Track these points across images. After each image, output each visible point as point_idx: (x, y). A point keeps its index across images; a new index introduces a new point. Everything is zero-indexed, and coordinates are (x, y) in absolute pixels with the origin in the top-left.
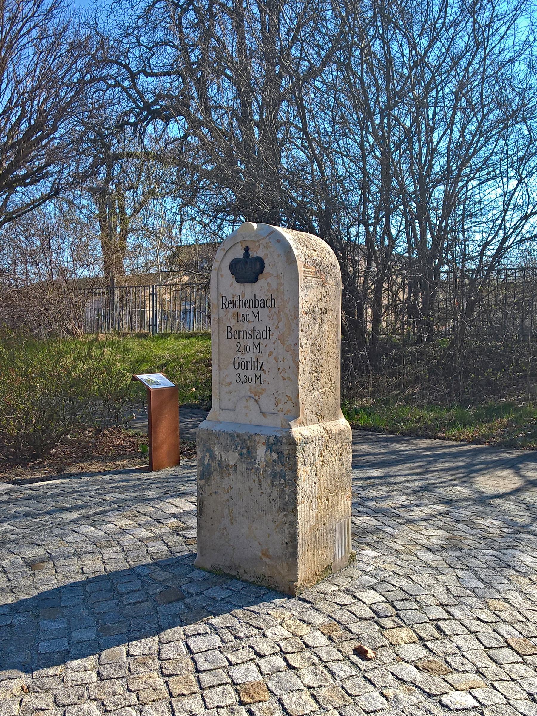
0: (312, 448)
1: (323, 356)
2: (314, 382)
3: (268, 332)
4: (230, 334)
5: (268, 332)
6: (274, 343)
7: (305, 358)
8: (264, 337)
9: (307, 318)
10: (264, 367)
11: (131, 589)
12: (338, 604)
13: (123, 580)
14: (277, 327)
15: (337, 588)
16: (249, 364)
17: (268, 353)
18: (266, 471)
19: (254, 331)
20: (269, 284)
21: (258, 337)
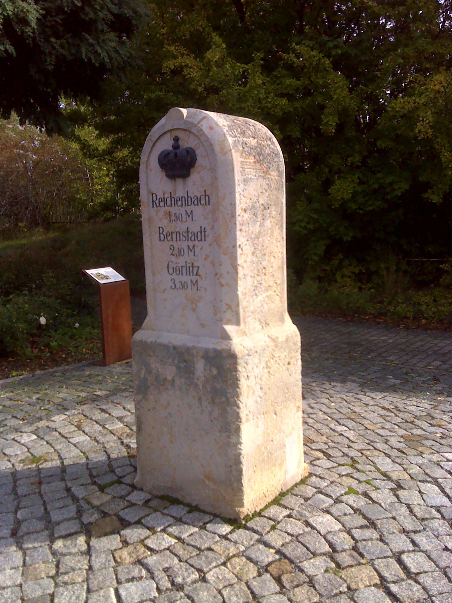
0: (256, 361)
1: (266, 257)
2: (256, 286)
3: (203, 233)
4: (162, 236)
5: (203, 233)
6: (210, 245)
8: (199, 239)
9: (246, 216)
10: (200, 272)
12: (289, 534)
13: (58, 505)
14: (213, 227)
15: (287, 512)
16: (184, 269)
17: (204, 257)
19: (188, 232)
21: (193, 239)
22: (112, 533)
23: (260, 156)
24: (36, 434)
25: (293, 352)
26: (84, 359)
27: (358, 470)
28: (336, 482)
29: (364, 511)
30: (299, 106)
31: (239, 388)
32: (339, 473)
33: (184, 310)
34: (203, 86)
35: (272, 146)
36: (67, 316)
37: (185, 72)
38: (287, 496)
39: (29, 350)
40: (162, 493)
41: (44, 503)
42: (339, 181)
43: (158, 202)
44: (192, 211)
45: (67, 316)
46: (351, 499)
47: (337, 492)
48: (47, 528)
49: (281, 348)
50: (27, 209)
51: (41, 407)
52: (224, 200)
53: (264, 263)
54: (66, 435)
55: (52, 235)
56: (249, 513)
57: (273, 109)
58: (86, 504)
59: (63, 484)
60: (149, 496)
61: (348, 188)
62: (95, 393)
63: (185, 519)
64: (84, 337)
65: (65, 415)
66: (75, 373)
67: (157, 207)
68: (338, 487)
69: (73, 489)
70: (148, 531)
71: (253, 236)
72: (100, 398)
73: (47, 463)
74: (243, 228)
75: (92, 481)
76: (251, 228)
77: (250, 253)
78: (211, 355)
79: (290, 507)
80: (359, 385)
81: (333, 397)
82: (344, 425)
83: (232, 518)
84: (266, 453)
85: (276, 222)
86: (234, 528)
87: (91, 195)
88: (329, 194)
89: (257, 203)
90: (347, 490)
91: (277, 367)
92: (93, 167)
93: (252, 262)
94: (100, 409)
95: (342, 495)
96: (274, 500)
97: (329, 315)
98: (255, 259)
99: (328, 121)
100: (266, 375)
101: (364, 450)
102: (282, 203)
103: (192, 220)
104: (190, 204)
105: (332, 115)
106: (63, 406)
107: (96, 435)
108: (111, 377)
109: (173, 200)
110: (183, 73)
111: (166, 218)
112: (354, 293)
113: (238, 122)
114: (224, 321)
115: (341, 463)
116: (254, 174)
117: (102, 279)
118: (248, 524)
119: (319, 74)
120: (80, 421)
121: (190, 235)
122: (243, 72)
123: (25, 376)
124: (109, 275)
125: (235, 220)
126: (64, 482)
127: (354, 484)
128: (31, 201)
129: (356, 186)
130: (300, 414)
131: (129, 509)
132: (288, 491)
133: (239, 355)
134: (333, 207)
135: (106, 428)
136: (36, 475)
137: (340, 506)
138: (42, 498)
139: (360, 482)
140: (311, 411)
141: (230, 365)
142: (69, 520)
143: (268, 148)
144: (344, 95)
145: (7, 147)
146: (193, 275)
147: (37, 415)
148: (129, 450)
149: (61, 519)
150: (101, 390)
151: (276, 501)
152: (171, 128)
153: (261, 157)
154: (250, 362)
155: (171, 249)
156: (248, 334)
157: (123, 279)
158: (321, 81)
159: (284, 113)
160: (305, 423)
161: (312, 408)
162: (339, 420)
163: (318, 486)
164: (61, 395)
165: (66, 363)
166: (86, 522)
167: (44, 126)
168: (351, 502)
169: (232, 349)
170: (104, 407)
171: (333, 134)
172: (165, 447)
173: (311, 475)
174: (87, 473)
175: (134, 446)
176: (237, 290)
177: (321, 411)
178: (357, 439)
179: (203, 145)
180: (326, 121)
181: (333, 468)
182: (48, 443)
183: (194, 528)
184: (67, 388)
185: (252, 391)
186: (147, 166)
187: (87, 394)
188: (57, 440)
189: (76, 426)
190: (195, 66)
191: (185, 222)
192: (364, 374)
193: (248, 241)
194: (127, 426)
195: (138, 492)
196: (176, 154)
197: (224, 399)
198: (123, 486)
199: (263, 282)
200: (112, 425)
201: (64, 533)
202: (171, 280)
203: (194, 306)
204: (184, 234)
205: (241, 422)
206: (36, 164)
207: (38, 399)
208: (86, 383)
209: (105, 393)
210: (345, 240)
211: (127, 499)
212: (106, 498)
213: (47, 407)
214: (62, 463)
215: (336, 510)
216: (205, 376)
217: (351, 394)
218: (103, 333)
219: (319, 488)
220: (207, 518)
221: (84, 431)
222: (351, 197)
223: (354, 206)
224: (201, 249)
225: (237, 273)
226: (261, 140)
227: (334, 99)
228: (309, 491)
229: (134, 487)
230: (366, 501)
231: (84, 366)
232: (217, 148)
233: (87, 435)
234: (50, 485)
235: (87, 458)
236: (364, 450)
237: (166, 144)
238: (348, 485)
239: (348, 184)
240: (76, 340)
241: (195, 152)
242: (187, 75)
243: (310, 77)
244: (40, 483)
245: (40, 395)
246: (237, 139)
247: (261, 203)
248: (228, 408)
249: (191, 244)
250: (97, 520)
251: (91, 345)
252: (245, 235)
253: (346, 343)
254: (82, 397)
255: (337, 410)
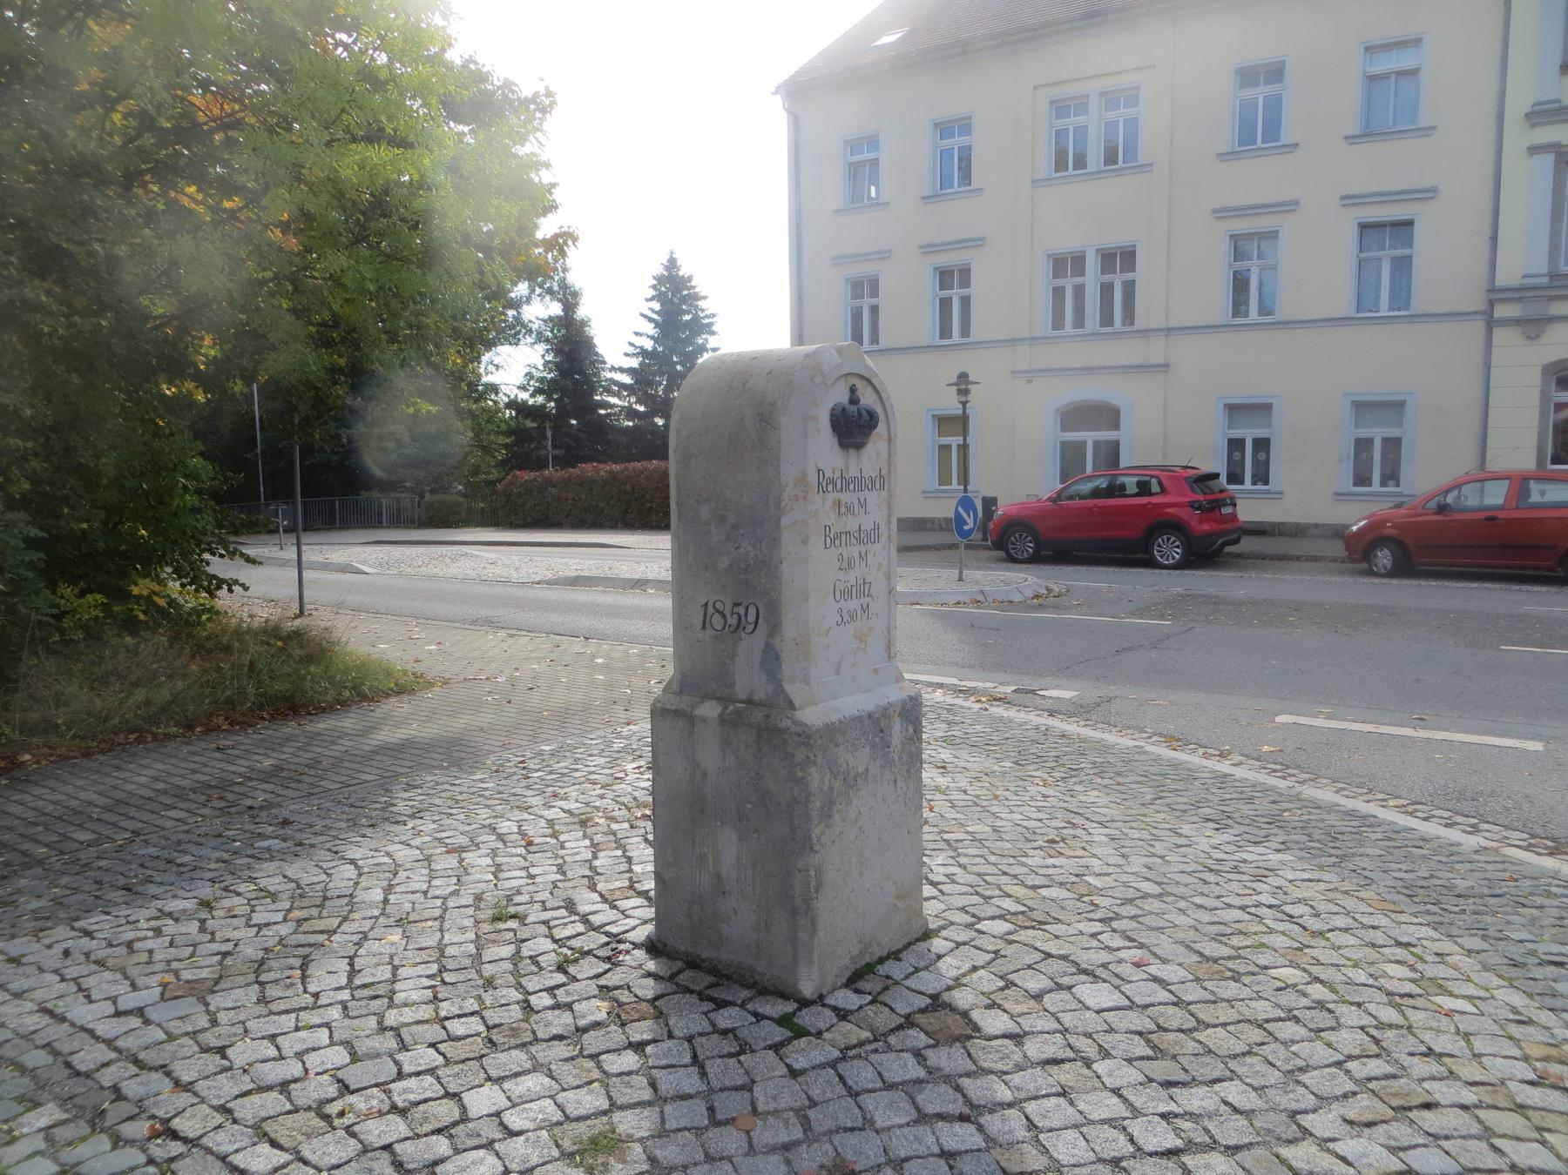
10: (873, 591)
164: (84, 795)
249: (863, 548)
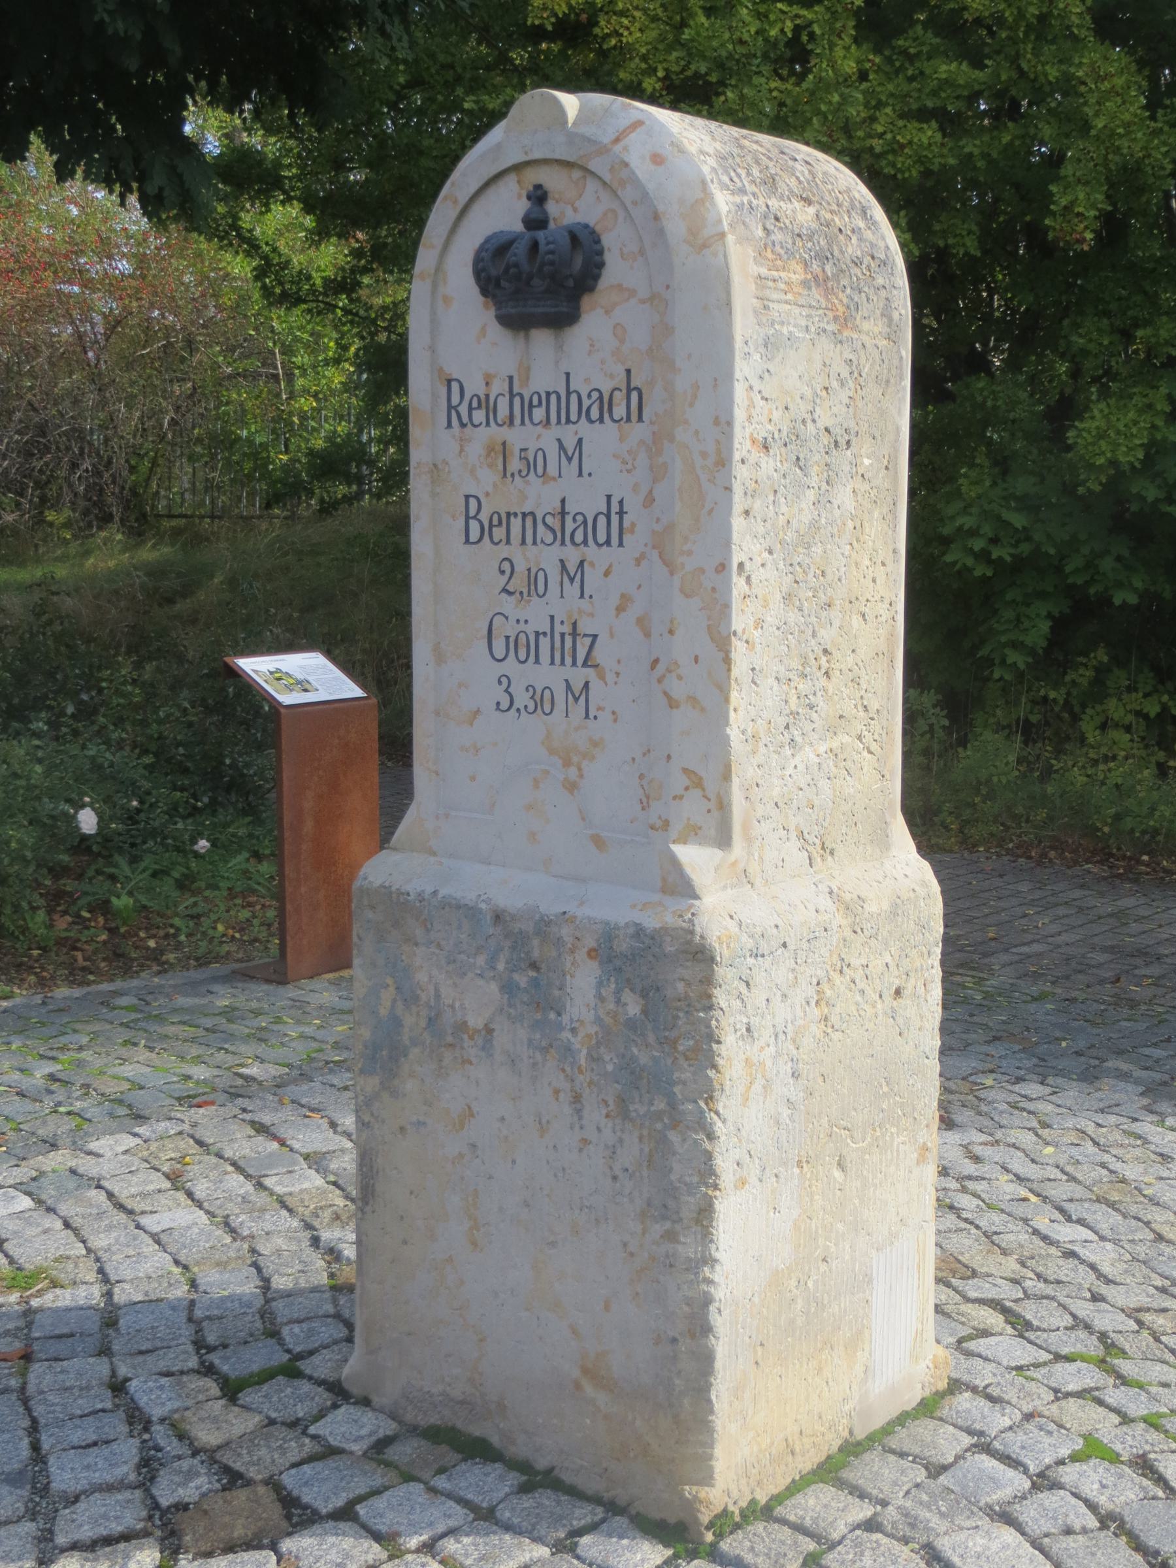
0: (782, 974)
1: (835, 614)
3: (615, 519)
4: (474, 526)
5: (615, 519)
6: (638, 561)
7: (759, 624)
8: (602, 538)
9: (769, 465)
10: (599, 655)
11: (97, 1477)
13: (76, 1437)
14: (649, 501)
15: (864, 1511)
16: (545, 643)
17: (615, 601)
18: (598, 1059)
19: (563, 513)
20: (619, 331)
21: (579, 537)
22: (250, 1545)
23: (826, 268)
24: (29, 1194)
25: (914, 953)
26: (217, 958)
27: (1123, 1380)
28: (1041, 1416)
29: (1136, 1524)
30: (976, 151)
31: (714, 1066)
32: (1054, 1385)
33: (536, 783)
34: (660, 74)
35: (868, 235)
36: (173, 811)
37: (604, 26)
38: (867, 1456)
39: (41, 915)
40: (434, 1419)
41: (34, 1428)
42: (1102, 405)
43: (465, 409)
44: (580, 441)
45: (173, 811)
46: (1091, 1478)
47: (1042, 1449)
48: (32, 1514)
49: (873, 937)
50: (74, 466)
51: (59, 1104)
52: (691, 405)
53: (827, 635)
54: (130, 1204)
55: (148, 554)
56: (731, 1508)
57: (890, 157)
58: (175, 1441)
59: (102, 1368)
60: (388, 1427)
61: (1134, 430)
62: (242, 1070)
63: (504, 1514)
64: (224, 884)
65: (135, 1135)
66: (182, 1001)
67: (463, 425)
68: (1050, 1433)
69: (133, 1386)
70: (376, 1547)
71: (790, 536)
72: (255, 1087)
73: (58, 1291)
74: (757, 505)
75: (202, 1363)
76: (784, 509)
77: (778, 596)
78: (623, 945)
79: (875, 1492)
80: (1141, 1089)
81: (1049, 1126)
82: (1081, 1222)
83: (672, 1520)
84: (800, 1304)
85: (874, 493)
86: (676, 1556)
87: (283, 427)
88: (1069, 448)
89: (809, 424)
90: (1079, 1444)
91: (857, 1004)
92: (297, 339)
93: (783, 627)
94: (252, 1123)
95: (1061, 1462)
96: (821, 1466)
97: (1052, 854)
98: (793, 617)
99: (1073, 203)
100: (816, 1030)
101: (1148, 1310)
102: (898, 430)
103: (580, 474)
104: (573, 418)
105: (1087, 183)
106: (130, 1106)
107: (232, 1208)
108: (298, 1022)
109: (517, 400)
110: (597, 31)
111: (490, 466)
112: (1139, 782)
113: (755, 147)
114: (676, 829)
115: (1065, 1351)
116: (803, 323)
117: (289, 688)
118: (724, 1546)
119: (1048, 50)
120: (181, 1160)
121: (570, 526)
122: (797, 29)
123: (18, 1000)
124: (310, 679)
125: (729, 476)
126: (105, 1359)
127: (1106, 1426)
128: (90, 444)
129: (1160, 422)
130: (930, 1171)
131: (319, 1465)
132: (871, 1438)
133: (722, 952)
134: (1081, 490)
135: (266, 1189)
136: (18, 1329)
137: (1051, 1499)
138: (29, 1410)
139: (1126, 1420)
140: (970, 1168)
141: (689, 984)
142: (110, 1488)
143: (854, 240)
144: (1127, 117)
145: (27, 269)
146: (574, 664)
147: (40, 1132)
148: (335, 1266)
149: (83, 1484)
150: (262, 1061)
151: (828, 1473)
152: (517, 157)
153: (829, 268)
154: (759, 977)
155: (503, 572)
156: (758, 882)
157: (358, 692)
158: (1053, 73)
159: (927, 173)
160: (946, 1207)
161: (977, 1159)
162: (1067, 1206)
163: (977, 1426)
164: (128, 1070)
165: (155, 968)
166: (164, 1502)
167: (135, 185)
168: (1090, 1489)
169: (698, 929)
170: (266, 1118)
171: (1086, 248)
172: (450, 1260)
173: (955, 1386)
174: (187, 1332)
175: (350, 1252)
176: (727, 724)
177: (1007, 1171)
178: (1126, 1271)
179: (629, 216)
180: (1064, 202)
181: (1037, 1366)
182: (67, 1225)
183: (534, 1546)
184: (151, 1049)
185: (759, 1083)
186: (435, 286)
187: (216, 1072)
188: (100, 1215)
189: (167, 1176)
190: (637, 8)
191: (554, 479)
192: (1158, 1053)
193: (770, 552)
194: (335, 1184)
195: (352, 1409)
196: (535, 246)
197: (660, 1105)
198: (305, 1387)
199: (819, 700)
200: (286, 1179)
201: (87, 1533)
202: (500, 682)
203: (573, 772)
204: (549, 520)
205: (716, 1187)
206: (114, 324)
207: (52, 1078)
208: (216, 1037)
209: (274, 1071)
210: (1117, 601)
211: (312, 1430)
212: (240, 1423)
213: (78, 1105)
214: (109, 1294)
215: (1041, 1512)
216: (598, 1020)
217: (1113, 1119)
218: (281, 873)
219: (981, 1434)
220: (583, 1514)
221: (190, 1195)
222: (1141, 462)
223: (1152, 493)
224: (607, 574)
225: (727, 661)
226: (832, 212)
227: (1093, 132)
228: (947, 1442)
229: (339, 1392)
230: (1142, 1488)
231: (215, 979)
232: (675, 228)
233: (200, 1207)
234: (58, 1366)
235: (193, 1284)
236: (1148, 1310)
237: (504, 213)
238: (1084, 1430)
239: (1132, 415)
240: (194, 893)
241: (598, 241)
242: (608, 35)
243: (1018, 55)
244: (27, 1357)
245: (59, 1067)
246: (745, 199)
247: (821, 424)
248: (673, 1136)
249: (572, 555)
250: (204, 1495)
251: (245, 914)
252: (761, 530)
253: (1105, 949)
254: (198, 1082)
255: (1063, 1171)
